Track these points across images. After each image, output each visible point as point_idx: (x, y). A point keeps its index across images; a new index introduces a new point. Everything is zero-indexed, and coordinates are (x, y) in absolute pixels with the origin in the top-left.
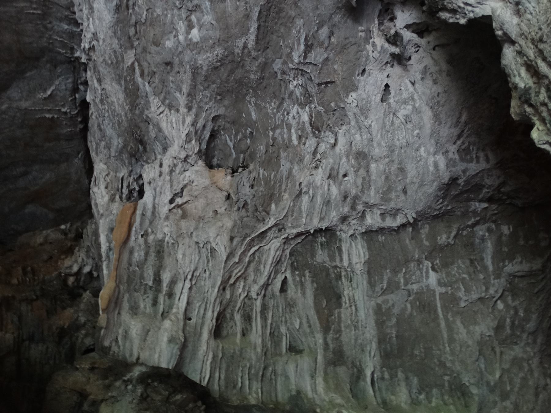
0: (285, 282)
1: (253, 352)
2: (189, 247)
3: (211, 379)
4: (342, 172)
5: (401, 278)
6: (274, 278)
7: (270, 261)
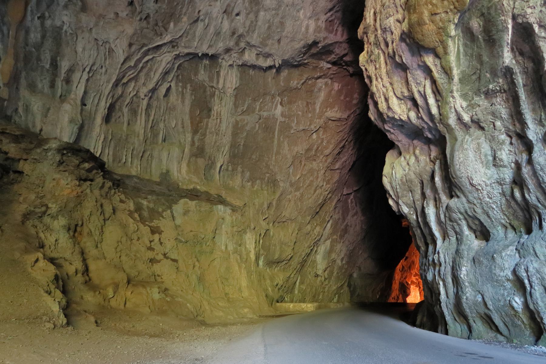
0: (169, 89)
1: (136, 138)
2: (89, 42)
3: (102, 154)
4: (236, 11)
5: (258, 105)
6: (161, 85)
7: (160, 71)
